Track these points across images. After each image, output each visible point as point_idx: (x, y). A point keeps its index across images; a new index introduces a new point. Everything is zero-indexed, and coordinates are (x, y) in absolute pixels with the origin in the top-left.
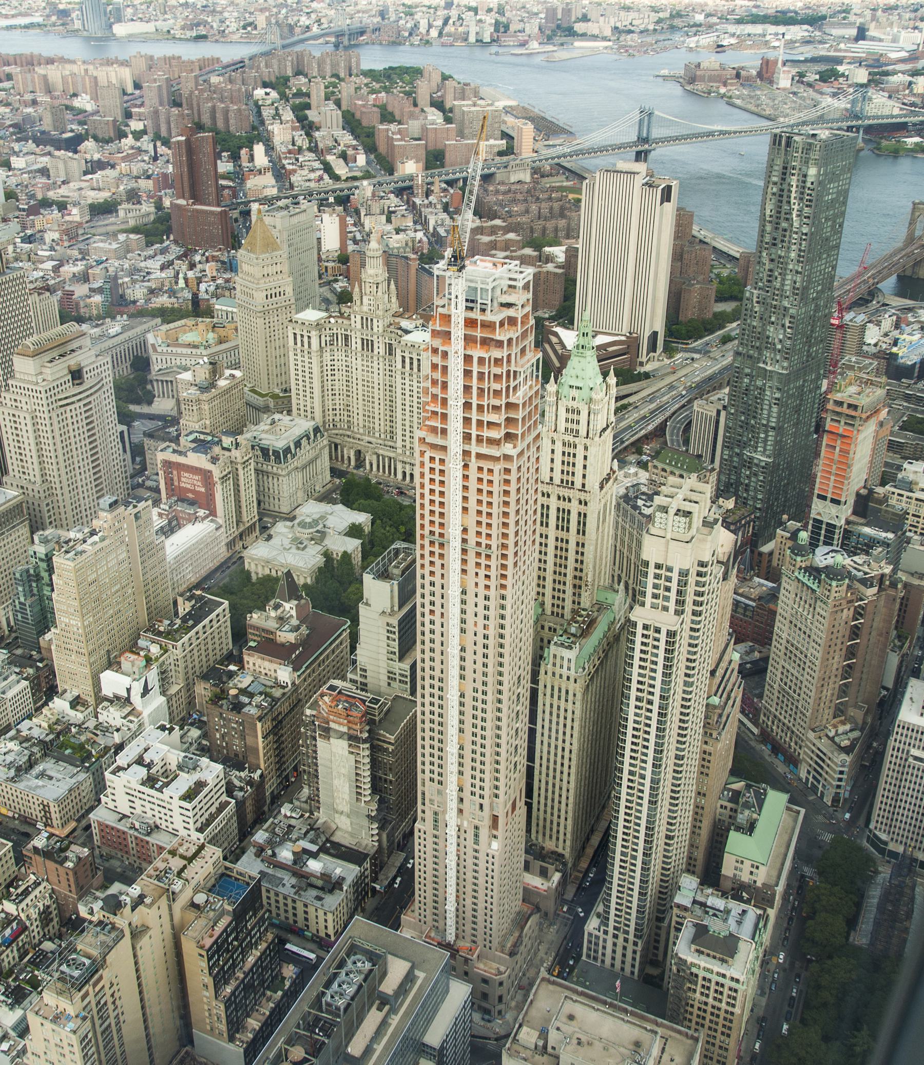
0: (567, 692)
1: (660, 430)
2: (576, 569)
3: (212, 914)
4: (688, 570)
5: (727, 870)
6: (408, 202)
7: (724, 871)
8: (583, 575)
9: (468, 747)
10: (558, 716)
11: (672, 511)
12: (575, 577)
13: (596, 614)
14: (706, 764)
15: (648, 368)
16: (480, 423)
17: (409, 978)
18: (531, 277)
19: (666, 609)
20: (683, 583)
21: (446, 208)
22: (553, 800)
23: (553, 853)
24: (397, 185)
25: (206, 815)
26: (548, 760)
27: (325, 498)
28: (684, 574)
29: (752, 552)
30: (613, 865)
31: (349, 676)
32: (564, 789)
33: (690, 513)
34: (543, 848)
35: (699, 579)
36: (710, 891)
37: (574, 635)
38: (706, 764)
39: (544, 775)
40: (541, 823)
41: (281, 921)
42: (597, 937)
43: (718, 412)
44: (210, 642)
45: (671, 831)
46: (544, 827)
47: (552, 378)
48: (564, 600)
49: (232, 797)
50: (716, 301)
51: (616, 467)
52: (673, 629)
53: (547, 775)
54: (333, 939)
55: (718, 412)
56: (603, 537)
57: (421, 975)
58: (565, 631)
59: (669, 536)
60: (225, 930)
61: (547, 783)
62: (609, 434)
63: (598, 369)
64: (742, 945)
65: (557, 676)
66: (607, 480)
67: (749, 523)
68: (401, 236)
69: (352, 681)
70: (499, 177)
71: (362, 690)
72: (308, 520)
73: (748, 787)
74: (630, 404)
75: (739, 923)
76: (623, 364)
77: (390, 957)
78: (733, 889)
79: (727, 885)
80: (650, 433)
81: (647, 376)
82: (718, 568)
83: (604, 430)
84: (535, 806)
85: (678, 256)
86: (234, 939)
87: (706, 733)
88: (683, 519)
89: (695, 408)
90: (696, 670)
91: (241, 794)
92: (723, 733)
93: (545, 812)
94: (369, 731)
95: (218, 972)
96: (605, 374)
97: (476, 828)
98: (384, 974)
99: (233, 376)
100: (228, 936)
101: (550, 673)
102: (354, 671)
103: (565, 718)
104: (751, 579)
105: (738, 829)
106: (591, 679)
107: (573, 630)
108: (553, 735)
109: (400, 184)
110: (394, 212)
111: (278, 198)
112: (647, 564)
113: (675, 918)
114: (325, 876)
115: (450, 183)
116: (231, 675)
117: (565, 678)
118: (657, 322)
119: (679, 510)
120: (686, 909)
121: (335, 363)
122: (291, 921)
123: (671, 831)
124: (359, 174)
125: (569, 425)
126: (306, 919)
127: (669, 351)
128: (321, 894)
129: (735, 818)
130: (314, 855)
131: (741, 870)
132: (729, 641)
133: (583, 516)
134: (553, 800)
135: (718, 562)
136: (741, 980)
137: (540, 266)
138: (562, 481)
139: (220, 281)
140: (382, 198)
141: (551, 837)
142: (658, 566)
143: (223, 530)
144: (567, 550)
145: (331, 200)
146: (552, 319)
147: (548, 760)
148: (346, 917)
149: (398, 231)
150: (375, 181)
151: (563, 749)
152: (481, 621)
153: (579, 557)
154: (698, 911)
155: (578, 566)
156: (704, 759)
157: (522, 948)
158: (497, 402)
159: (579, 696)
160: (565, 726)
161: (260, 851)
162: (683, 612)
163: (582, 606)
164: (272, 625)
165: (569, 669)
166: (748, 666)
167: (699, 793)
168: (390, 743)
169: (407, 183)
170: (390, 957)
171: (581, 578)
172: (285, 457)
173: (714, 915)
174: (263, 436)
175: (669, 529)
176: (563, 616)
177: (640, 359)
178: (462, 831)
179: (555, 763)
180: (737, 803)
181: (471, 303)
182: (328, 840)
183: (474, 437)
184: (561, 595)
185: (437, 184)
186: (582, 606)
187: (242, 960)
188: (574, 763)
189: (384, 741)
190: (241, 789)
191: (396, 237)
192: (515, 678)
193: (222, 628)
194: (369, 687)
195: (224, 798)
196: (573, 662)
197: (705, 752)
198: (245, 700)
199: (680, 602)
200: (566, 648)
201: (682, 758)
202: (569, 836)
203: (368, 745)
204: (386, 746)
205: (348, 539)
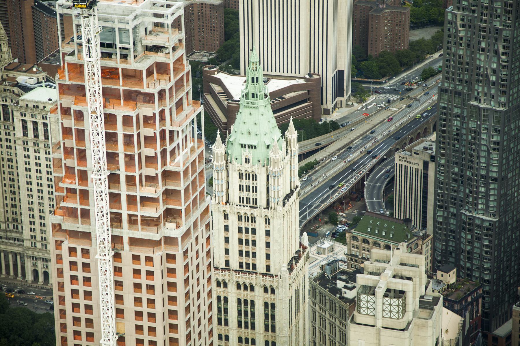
11: (380, 292)
15: (335, 116)
18: (181, 12)
29: (485, 336)
33: (403, 292)
43: (426, 165)
47: (218, 138)
51: (306, 242)
62: (294, 202)
66: (297, 258)
67: (476, 300)
74: (317, 163)
76: (303, 113)
80: (345, 196)
81: (334, 126)
83: (288, 197)
88: (395, 302)
89: (397, 161)
96: (283, 128)
119: (388, 290)
127: (359, 93)
133: (270, 308)
138: (241, 265)
146: (212, 63)
158: (150, 172)
175: (379, 315)
177: (324, 106)
183: (125, 218)
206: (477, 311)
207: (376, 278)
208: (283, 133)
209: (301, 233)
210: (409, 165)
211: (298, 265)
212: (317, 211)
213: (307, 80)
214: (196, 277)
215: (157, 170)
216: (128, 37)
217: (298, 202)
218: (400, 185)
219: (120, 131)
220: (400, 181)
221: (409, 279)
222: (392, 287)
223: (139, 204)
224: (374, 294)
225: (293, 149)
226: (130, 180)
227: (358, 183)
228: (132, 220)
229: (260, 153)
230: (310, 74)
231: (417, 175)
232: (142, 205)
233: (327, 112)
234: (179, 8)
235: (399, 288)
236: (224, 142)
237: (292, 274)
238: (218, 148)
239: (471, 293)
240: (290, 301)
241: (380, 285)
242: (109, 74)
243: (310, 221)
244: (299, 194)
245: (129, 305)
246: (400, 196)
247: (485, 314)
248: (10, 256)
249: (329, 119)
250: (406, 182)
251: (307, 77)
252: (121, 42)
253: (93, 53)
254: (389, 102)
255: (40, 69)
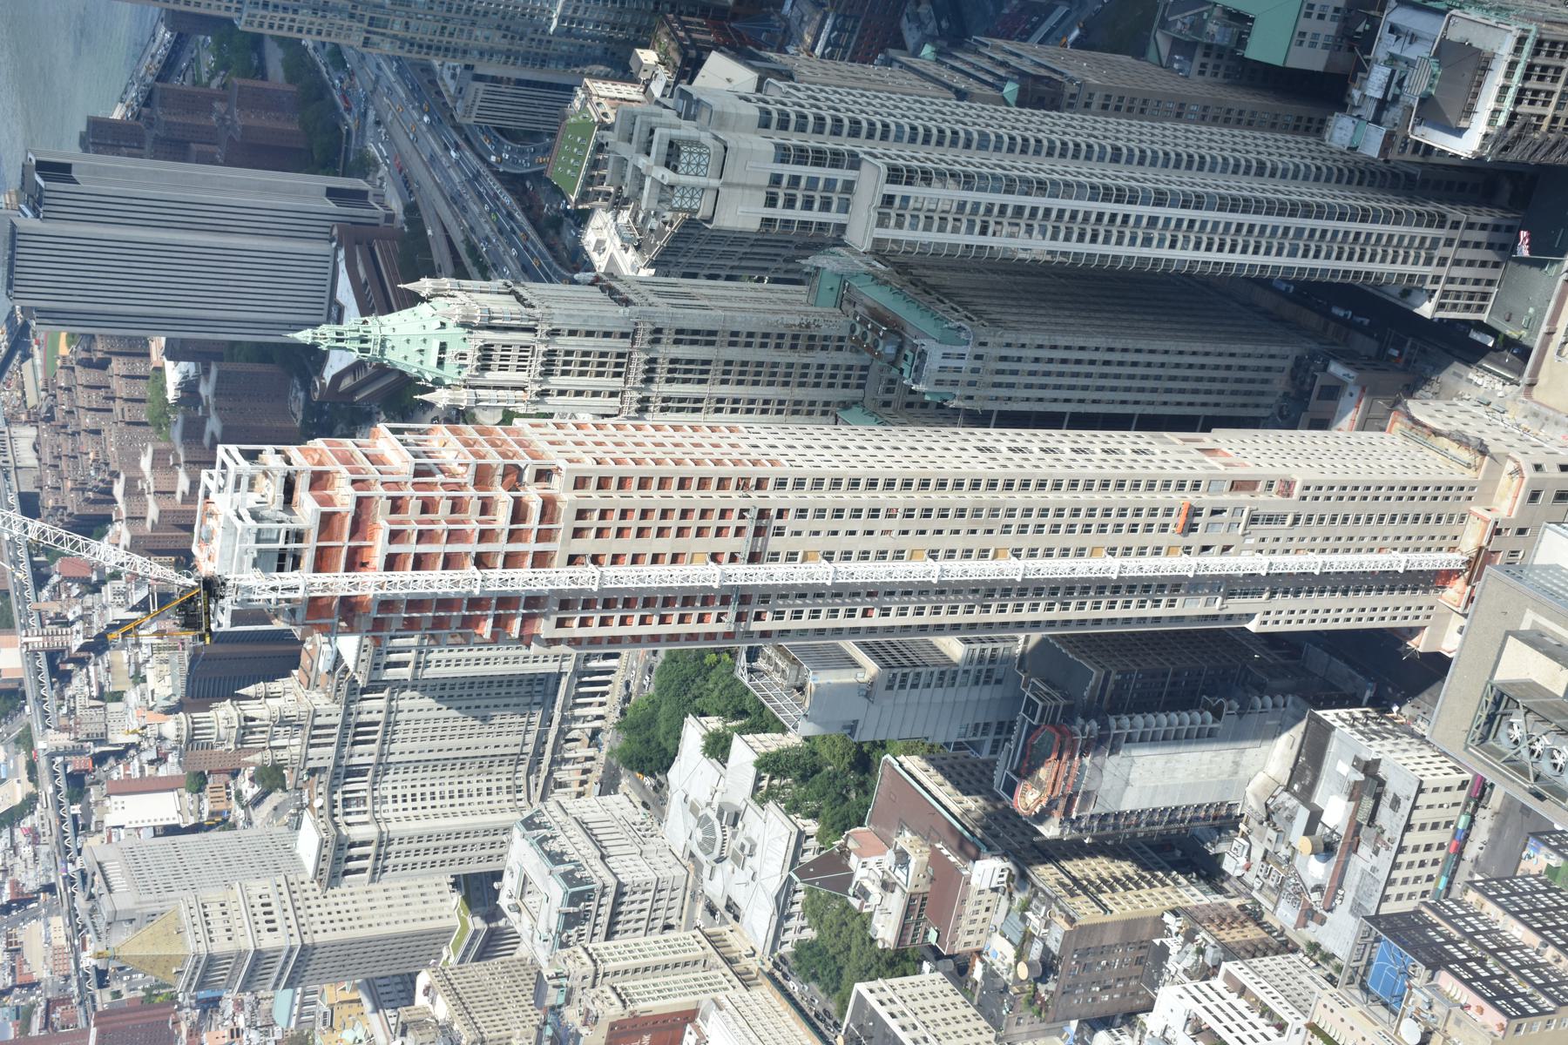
0: (1004, 359)
1: (513, 182)
3: (1438, 1009)
4: (777, 146)
5: (1314, 60)
6: (81, 663)
7: (1319, 66)
8: (789, 332)
9: (1110, 538)
11: (668, 176)
12: (794, 347)
13: (859, 309)
14: (1125, 104)
15: (396, 206)
17: (1535, 640)
18: (233, 448)
19: (849, 186)
20: (801, 156)
21: (96, 588)
23: (1293, 377)
25: (1254, 1017)
26: (1128, 389)
28: (783, 154)
29: (735, 17)
30: (1313, 271)
33: (671, 144)
34: (1286, 394)
35: (792, 125)
36: (1356, 94)
37: (900, 349)
38: (1125, 104)
40: (1240, 400)
41: (1442, 872)
42: (1445, 294)
43: (479, 78)
44: (932, 1015)
45: (1248, 167)
47: (425, 397)
48: (836, 367)
49: (1217, 967)
50: (264, 78)
51: (589, 276)
52: (884, 170)
54: (1468, 776)
55: (479, 78)
56: (717, 298)
57: (1529, 620)
58: (893, 363)
59: (715, 182)
60: (1467, 983)
62: (530, 289)
64: (1455, 35)
65: (975, 377)
66: (612, 292)
67: (683, 24)
68: (150, 673)
70: (28, 488)
71: (1010, 730)
72: (699, 835)
73: (1164, 24)
74: (467, 241)
75: (1414, 38)
76: (393, 264)
78: (1351, 49)
79: (1344, 61)
80: (519, 201)
81: (411, 209)
82: (771, 90)
83: (520, 299)
84: (1210, 411)
85: (176, 147)
86: (1483, 966)
87: (1070, 106)
88: (684, 158)
89: (471, 121)
90: (958, 127)
91: (1210, 951)
92: (1070, 74)
93: (1220, 392)
94: (1086, 718)
95: (1549, 995)
96: (414, 299)
97: (1254, 520)
98: (1531, 687)
99: (427, 991)
100: (1477, 977)
101: (970, 391)
102: (976, 746)
103: (1051, 361)
104: (784, 19)
105: (1242, 42)
107: (890, 350)
108: (1082, 381)
109: (45, 677)
110: (101, 687)
111: (72, 913)
112: (768, 222)
113: (1408, 156)
114: (1355, 793)
115: (40, 580)
116: (990, 974)
117: (978, 364)
118: (305, 191)
119: (667, 165)
120: (1389, 137)
122: (1441, 855)
123: (1248, 167)
124: (22, 759)
126: (1435, 826)
127: (364, 166)
128: (1386, 801)
129: (1222, 48)
130: (1315, 816)
131: (1315, 36)
132: (903, 65)
133: (684, 336)
135: (759, 90)
136: (1519, 34)
138: (618, 375)
139: (241, 1022)
140: (72, 711)
142: (771, 201)
143: (721, 996)
145: (76, 809)
146: (307, 386)
147: (1128, 389)
148: (1428, 752)
149: (139, 678)
150: (37, 727)
151: (1106, 363)
152: (881, 523)
154: (1393, 114)
155: (772, 342)
156: (1118, 108)
157: (1471, 432)
158: (474, 506)
159: (1009, 337)
160: (1064, 361)
161: (1309, 915)
162: (853, 155)
163: (845, 332)
164: (896, 902)
165: (961, 356)
166: (944, 24)
167: (1179, 115)
168: (1106, 679)
169: (43, 663)
170: (1499, 677)
171: (795, 337)
172: (581, 882)
173: (1400, 84)
174: (542, 926)
175: (702, 181)
177: (381, 221)
178: (1262, 546)
180: (1195, 44)
182: (1288, 788)
183: (541, 547)
185: (42, 606)
186: (845, 332)
187: (1521, 948)
188: (1131, 344)
189: (1104, 688)
190: (1201, 951)
191: (152, 682)
193: (905, 994)
194: (1005, 718)
195: (1218, 983)
196: (949, 349)
197: (1105, 107)
198: (1035, 952)
199: (837, 159)
200: (924, 362)
201: (1117, 149)
202: (1262, 349)
203: (1112, 721)
204: (1111, 686)
206: (700, 25)
207: (648, 182)
208: (423, 300)
209: (576, 282)
210: (478, 103)
212: (540, 246)
213: (339, 246)
215: (471, 493)
216: (270, 530)
217: (529, 284)
218: (508, 119)
219: (411, 548)
220: (502, 118)
221: (652, 132)
222: (663, 159)
224: (672, 187)
226: (484, 536)
227: (501, 181)
228: (544, 536)
229: (454, 334)
230: (331, 241)
231: (493, 93)
232: (523, 521)
233: (390, 218)
235: (665, 148)
236: (433, 390)
238: (441, 398)
239: (673, 30)
240: (673, 305)
241: (659, 177)
242: (322, 562)
244: (517, 282)
245: (667, 545)
246: (525, 120)
247: (704, 15)
248: (581, 690)
249: (400, 216)
250: (503, 110)
252: (277, 540)
254: (378, 123)
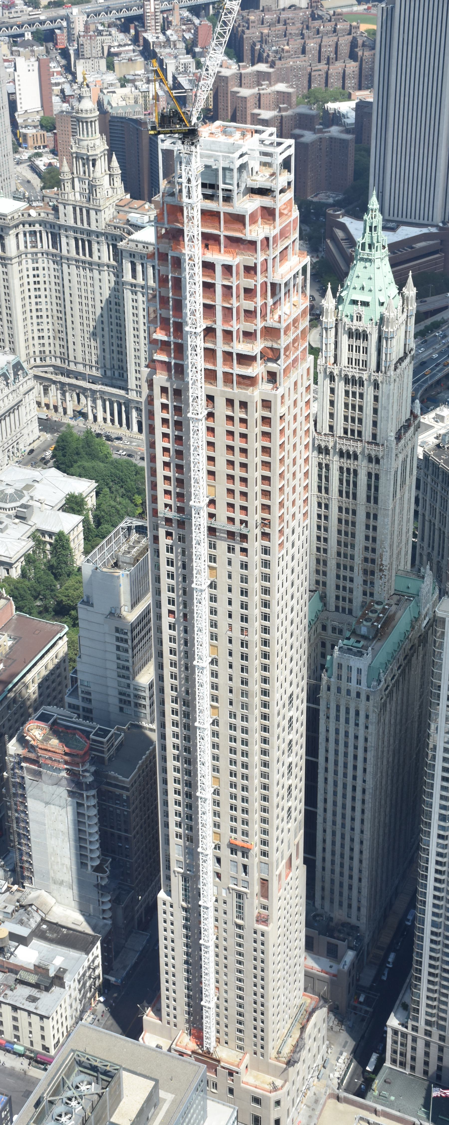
0: (357, 713)
2: (366, 549)
6: (135, 40)
8: (376, 556)
10: (346, 745)
12: (366, 560)
13: (394, 608)
16: (228, 355)
18: (292, 151)
21: (189, 51)
22: (342, 856)
23: (344, 924)
24: (122, 14)
26: (335, 803)
27: (34, 459)
31: (68, 700)
32: (357, 840)
34: (331, 919)
39: (329, 823)
40: (327, 886)
46: (332, 892)
47: (329, 292)
48: (351, 591)
53: (334, 823)
57: (166, 1096)
58: (354, 632)
61: (334, 833)
62: (408, 368)
63: (391, 276)
65: (344, 692)
66: (406, 427)
69: (71, 706)
71: (86, 718)
77: (125, 1075)
83: (401, 360)
84: (319, 864)
93: (333, 871)
94: (95, 774)
96: (401, 284)
97: (240, 896)
101: (333, 689)
102: (74, 693)
106: (390, 695)
107: (364, 631)
110: (117, 54)
114: (40, 969)
117: (354, 694)
121: (40, 272)
125: (354, 355)
126: (16, 1028)
128: (34, 992)
130: (23, 941)
133: (374, 479)
134: (342, 856)
137: (320, 131)
138: (346, 432)
141: (341, 904)
144: (354, 524)
145: (28, 36)
146: (337, 205)
147: (335, 803)
148: (70, 1023)
149: (124, 82)
151: (354, 788)
153: (371, 533)
155: (370, 544)
158: (249, 327)
159: (373, 717)
163: (376, 598)
165: (359, 682)
168: (123, 788)
170: (125, 1075)
171: (373, 561)
176: (350, 612)
178: (221, 902)
179: (344, 807)
181: (210, 189)
182: (43, 921)
183: (220, 376)
184: (348, 585)
185: (177, 11)
186: (376, 598)
189: (116, 786)
191: (121, 92)
192: (286, 697)
196: (364, 673)
203: (93, 792)
204: (118, 791)
205: (62, 514)
208: (400, 289)
211: (407, 435)
212: (440, 375)
214: (292, 442)
216: (232, 178)
223: (235, 361)
225: (410, 308)
230: (443, 222)
232: (239, 363)
234: (290, 146)
236: (334, 296)
237: (400, 445)
243: (431, 385)
251: (441, 225)
252: (225, 183)
253: (194, 194)
255: (153, 206)
